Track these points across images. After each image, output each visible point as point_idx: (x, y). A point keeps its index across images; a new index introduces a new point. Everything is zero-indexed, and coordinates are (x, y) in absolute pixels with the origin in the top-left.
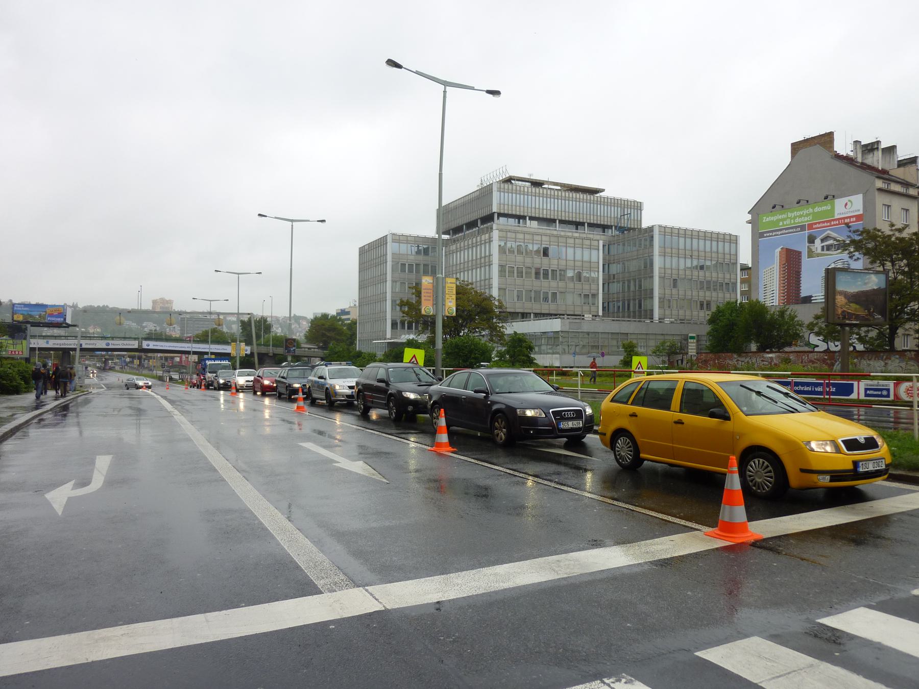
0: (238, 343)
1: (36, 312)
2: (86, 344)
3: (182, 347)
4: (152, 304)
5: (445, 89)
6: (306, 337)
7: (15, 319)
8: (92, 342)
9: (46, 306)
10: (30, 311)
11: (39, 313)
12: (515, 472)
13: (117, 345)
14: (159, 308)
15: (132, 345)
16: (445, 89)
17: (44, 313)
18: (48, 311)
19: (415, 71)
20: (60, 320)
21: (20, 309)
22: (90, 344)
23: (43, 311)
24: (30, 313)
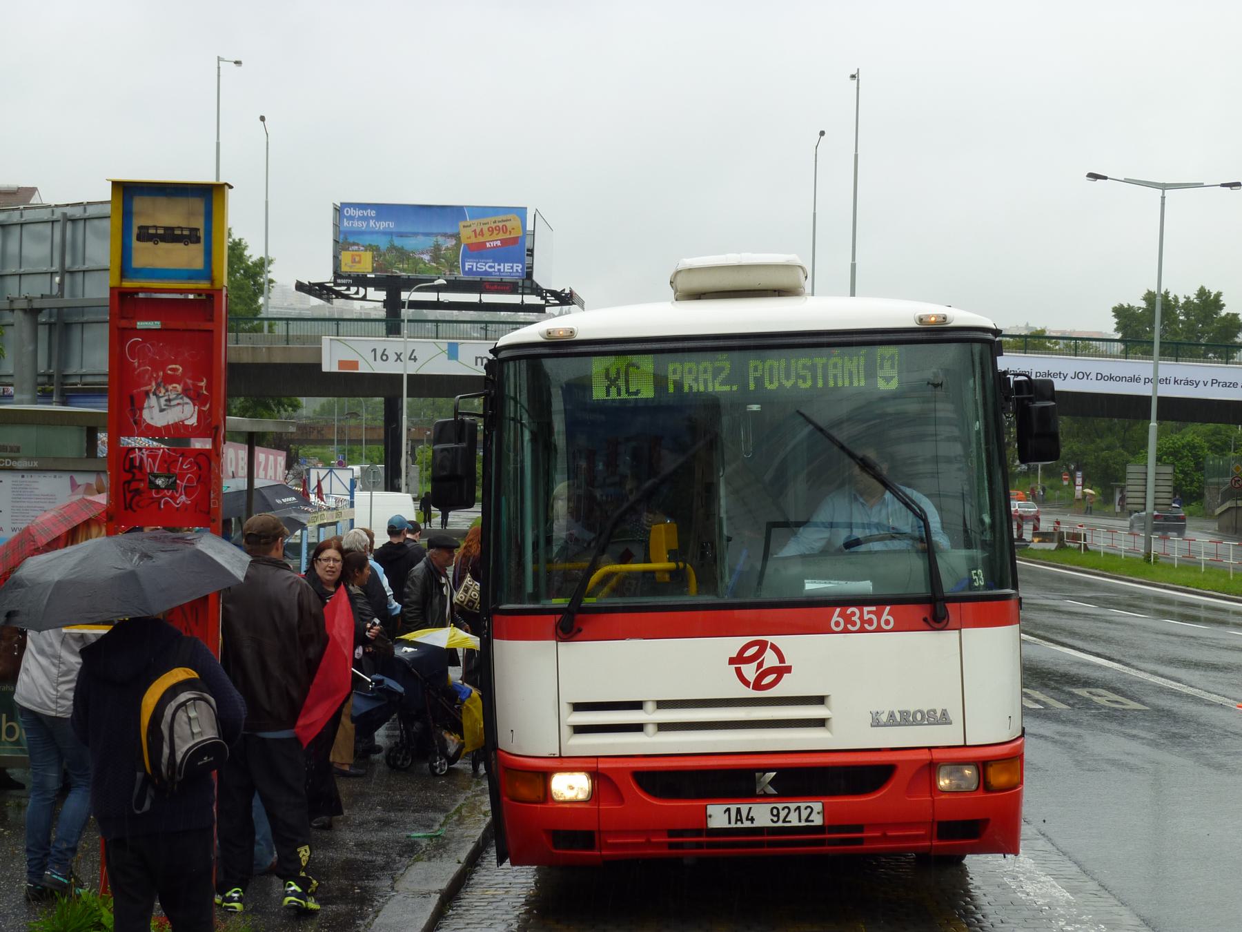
1: (421, 238)
5: (1163, 193)
6: (471, 506)
7: (345, 269)
10: (401, 235)
11: (430, 242)
16: (1163, 193)
17: (451, 243)
18: (467, 236)
19: (1123, 179)
20: (510, 270)
23: (445, 235)
24: (398, 242)
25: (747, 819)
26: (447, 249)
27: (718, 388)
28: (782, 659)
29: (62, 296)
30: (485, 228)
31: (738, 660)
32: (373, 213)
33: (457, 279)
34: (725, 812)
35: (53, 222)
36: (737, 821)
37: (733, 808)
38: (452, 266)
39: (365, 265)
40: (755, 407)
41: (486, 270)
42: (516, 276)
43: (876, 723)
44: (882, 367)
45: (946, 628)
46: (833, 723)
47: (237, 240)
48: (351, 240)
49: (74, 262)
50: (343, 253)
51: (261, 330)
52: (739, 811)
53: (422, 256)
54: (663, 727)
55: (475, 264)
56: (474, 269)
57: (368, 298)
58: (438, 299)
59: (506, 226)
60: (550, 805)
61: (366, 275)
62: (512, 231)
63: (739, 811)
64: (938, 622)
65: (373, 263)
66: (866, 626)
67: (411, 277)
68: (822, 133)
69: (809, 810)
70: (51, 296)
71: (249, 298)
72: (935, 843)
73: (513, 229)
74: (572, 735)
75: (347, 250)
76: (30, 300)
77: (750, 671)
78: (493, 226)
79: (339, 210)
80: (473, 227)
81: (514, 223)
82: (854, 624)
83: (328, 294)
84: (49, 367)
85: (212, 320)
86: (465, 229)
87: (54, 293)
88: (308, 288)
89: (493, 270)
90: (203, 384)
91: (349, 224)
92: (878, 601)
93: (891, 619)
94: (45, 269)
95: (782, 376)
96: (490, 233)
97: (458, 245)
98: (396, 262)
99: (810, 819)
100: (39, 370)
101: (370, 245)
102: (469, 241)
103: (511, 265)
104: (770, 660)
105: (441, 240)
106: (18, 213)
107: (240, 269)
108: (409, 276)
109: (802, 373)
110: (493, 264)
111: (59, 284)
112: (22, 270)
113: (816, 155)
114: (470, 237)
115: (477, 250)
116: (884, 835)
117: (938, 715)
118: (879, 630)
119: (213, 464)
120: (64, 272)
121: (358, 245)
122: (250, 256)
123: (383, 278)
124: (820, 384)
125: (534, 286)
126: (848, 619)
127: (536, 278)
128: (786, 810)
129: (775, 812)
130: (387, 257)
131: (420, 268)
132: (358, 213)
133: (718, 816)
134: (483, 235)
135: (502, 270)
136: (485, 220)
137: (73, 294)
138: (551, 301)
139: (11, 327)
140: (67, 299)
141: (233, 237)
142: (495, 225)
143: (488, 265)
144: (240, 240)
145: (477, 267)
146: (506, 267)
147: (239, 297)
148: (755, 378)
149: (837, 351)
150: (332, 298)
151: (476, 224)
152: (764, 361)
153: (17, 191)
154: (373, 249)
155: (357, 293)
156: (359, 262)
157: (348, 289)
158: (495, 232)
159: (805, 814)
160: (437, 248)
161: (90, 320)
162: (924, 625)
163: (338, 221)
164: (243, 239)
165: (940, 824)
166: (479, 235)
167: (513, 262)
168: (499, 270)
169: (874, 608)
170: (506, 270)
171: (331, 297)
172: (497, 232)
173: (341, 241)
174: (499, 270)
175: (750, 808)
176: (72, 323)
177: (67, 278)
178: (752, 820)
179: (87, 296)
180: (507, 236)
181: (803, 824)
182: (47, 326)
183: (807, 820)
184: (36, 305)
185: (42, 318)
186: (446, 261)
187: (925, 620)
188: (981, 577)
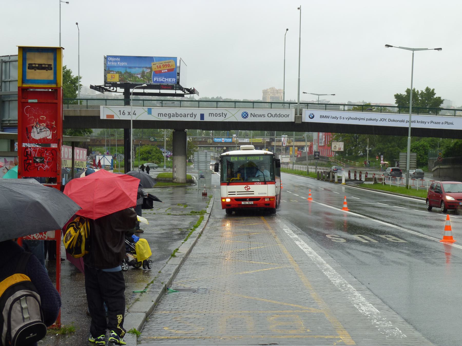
0: (294, 147)
1: (137, 69)
2: (211, 114)
3: (371, 120)
4: (262, 93)
7: (108, 80)
8: (219, 111)
9: (151, 59)
11: (140, 70)
12: (401, 228)
13: (260, 116)
14: (269, 99)
15: (284, 116)
17: (149, 70)
18: (154, 68)
20: (171, 81)
21: (115, 64)
22: (216, 115)
23: (146, 68)
24: (129, 70)
26: (147, 73)
30: (161, 65)
38: (149, 79)
39: (116, 79)
47: (68, 70)
48: (111, 69)
49: (6, 78)
50: (108, 74)
51: (77, 104)
53: (138, 76)
55: (158, 78)
56: (157, 81)
73: (172, 65)
78: (164, 64)
79: (106, 58)
80: (157, 65)
81: (172, 63)
83: (102, 90)
90: (54, 123)
97: (151, 71)
102: (155, 70)
105: (145, 69)
107: (69, 80)
115: (158, 73)
121: (113, 71)
132: (113, 59)
134: (160, 68)
135: (168, 81)
137: (5, 90)
141: (67, 69)
142: (165, 64)
145: (158, 80)
146: (169, 80)
147: (69, 91)
150: (104, 91)
151: (158, 63)
154: (120, 73)
155: (113, 89)
156: (114, 78)
157: (110, 88)
158: (165, 66)
160: (143, 72)
168: (167, 81)
170: (169, 81)
173: (107, 70)
174: (167, 81)
180: (170, 68)
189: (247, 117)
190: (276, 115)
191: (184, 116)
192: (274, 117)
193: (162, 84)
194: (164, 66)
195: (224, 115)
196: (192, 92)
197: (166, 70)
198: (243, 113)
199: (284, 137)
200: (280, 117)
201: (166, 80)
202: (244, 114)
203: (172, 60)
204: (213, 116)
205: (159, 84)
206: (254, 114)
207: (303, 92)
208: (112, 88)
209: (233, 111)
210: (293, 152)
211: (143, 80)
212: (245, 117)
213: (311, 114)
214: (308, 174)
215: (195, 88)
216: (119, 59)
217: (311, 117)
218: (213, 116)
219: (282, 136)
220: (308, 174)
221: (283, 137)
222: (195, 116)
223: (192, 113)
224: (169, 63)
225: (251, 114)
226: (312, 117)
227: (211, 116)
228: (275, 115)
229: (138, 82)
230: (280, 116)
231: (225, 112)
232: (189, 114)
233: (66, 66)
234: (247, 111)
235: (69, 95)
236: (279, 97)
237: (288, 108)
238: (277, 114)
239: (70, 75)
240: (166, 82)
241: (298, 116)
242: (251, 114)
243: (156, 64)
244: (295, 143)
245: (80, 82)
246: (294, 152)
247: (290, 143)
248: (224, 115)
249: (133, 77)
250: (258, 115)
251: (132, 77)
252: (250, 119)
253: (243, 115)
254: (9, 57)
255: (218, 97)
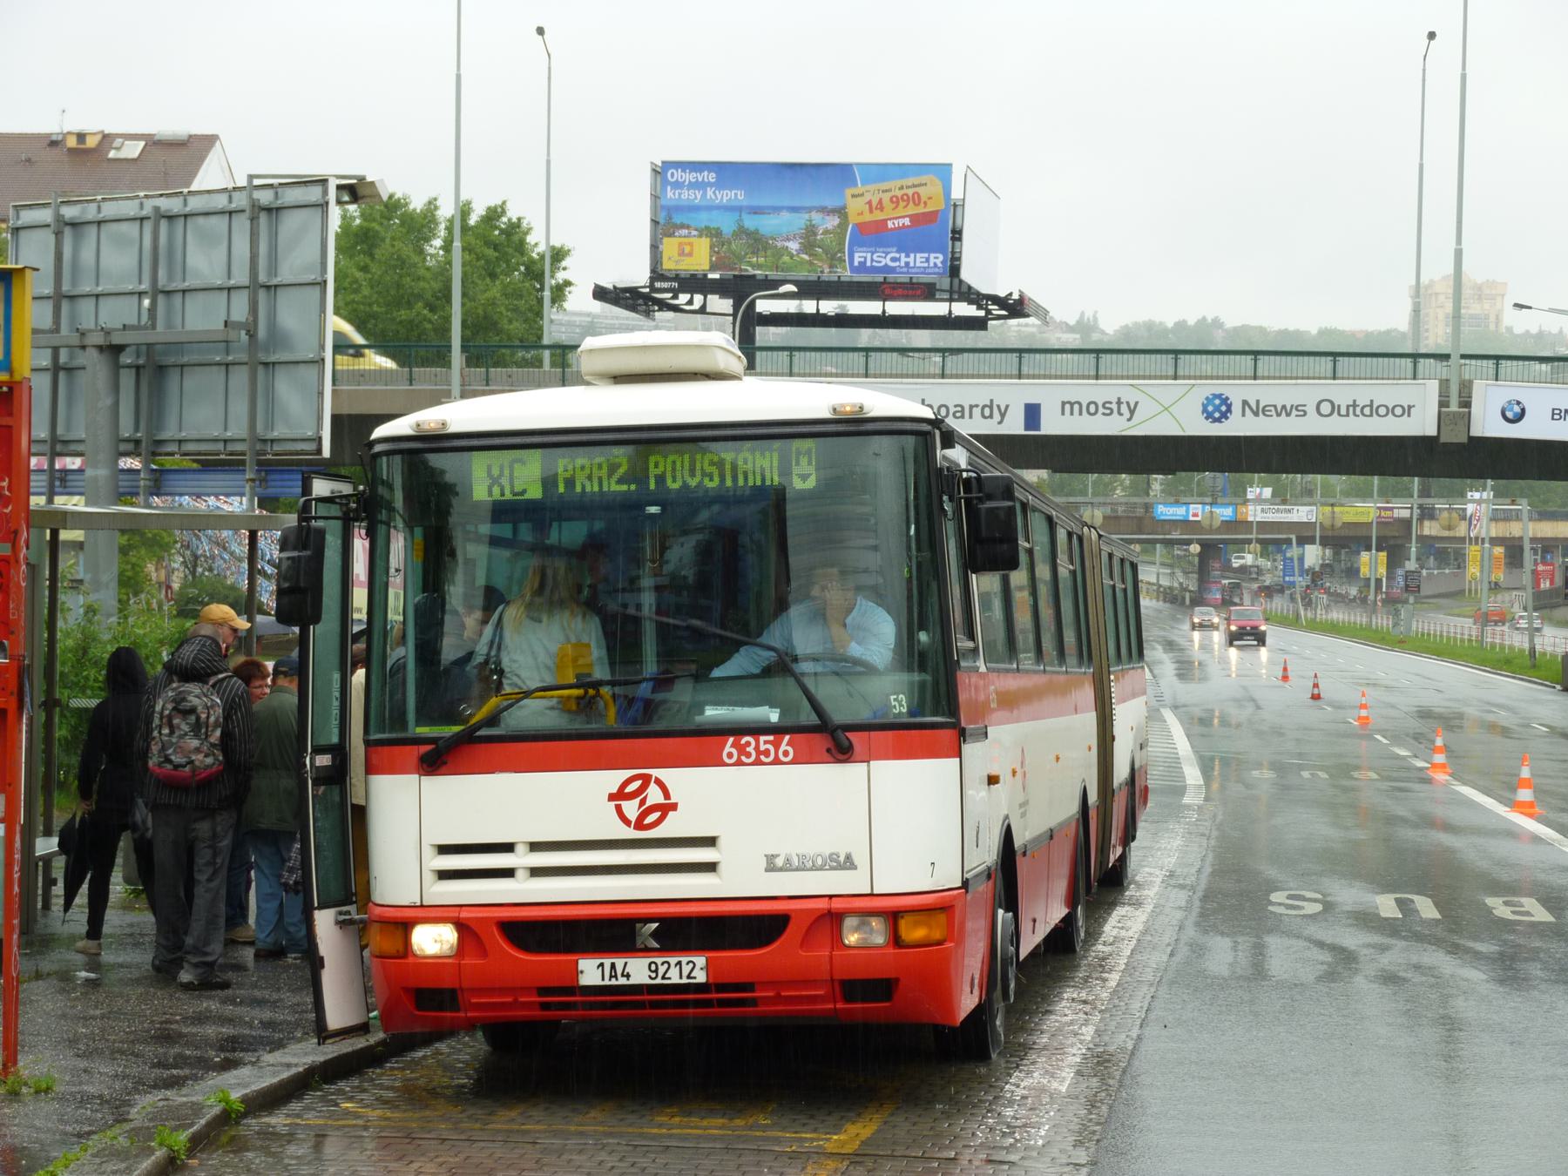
0: (1374, 551)
1: (786, 215)
2: (1068, 406)
7: (668, 265)
9: (838, 174)
10: (756, 211)
11: (799, 222)
13: (1284, 411)
15: (1390, 411)
17: (832, 222)
18: (857, 210)
20: (926, 263)
21: (694, 196)
22: (1092, 409)
24: (750, 222)
25: (623, 975)
26: (826, 232)
27: (615, 487)
28: (667, 795)
29: (154, 327)
30: (886, 197)
31: (619, 796)
32: (712, 177)
33: (842, 279)
34: (598, 967)
35: (142, 219)
36: (611, 977)
37: (607, 962)
38: (834, 259)
39: (698, 258)
40: (653, 510)
41: (886, 264)
42: (934, 274)
43: (771, 867)
44: (798, 463)
45: (852, 759)
46: (721, 868)
47: (514, 220)
48: (678, 219)
49: (170, 278)
50: (665, 240)
51: (540, 365)
52: (613, 966)
53: (787, 244)
54: (536, 872)
55: (869, 255)
56: (868, 264)
57: (708, 310)
58: (818, 310)
59: (918, 195)
60: (410, 960)
61: (705, 275)
62: (929, 202)
63: (613, 966)
64: (844, 754)
65: (711, 256)
66: (762, 757)
67: (769, 278)
68: (1432, 36)
69: (691, 965)
70: (133, 328)
71: (531, 309)
72: (839, 1006)
73: (930, 198)
74: (435, 882)
75: (671, 235)
76: (107, 332)
77: (631, 809)
78: (899, 193)
79: (660, 172)
80: (867, 197)
81: (931, 189)
82: (748, 755)
83: (646, 304)
84: (137, 429)
85: (10, 414)
86: (855, 199)
87: (143, 323)
88: (613, 295)
89: (897, 264)
90: (5, 484)
91: (674, 194)
92: (777, 731)
93: (790, 750)
94: (131, 287)
95: (686, 473)
96: (894, 205)
97: (843, 226)
98: (747, 254)
99: (692, 975)
100: (120, 433)
101: (707, 228)
102: (860, 219)
103: (926, 255)
104: (654, 795)
105: (816, 217)
106: (93, 206)
107: (518, 264)
108: (766, 276)
109: (708, 469)
110: (897, 255)
111: (149, 310)
112: (100, 289)
113: (1424, 70)
114: (862, 213)
115: (874, 233)
116: (778, 995)
117: (842, 859)
118: (777, 762)
119: (12, 571)
120: (156, 292)
121: (688, 227)
122: (536, 244)
123: (729, 280)
124: (729, 483)
125: (964, 289)
126: (742, 750)
127: (966, 275)
128: (666, 966)
129: (653, 967)
130: (734, 246)
131: (784, 263)
132: (689, 177)
133: (591, 971)
134: (882, 209)
135: (912, 264)
136: (885, 186)
137: (169, 325)
138: (994, 312)
139: (82, 371)
140: (160, 334)
141: (509, 214)
142: (902, 192)
143: (889, 257)
144: (519, 219)
145: (872, 260)
146: (918, 260)
147: (516, 310)
148: (656, 476)
149: (748, 444)
150: (654, 311)
151: (872, 192)
152: (666, 457)
153: (188, 141)
154: (713, 234)
155: (690, 302)
156: (690, 254)
157: (675, 297)
158: (902, 204)
159: (686, 969)
160: (811, 230)
161: (192, 362)
162: (826, 755)
163: (659, 188)
164: (524, 218)
165: (843, 983)
166: (876, 208)
167: (930, 251)
168: (907, 264)
169: (771, 738)
170: (918, 264)
171: (651, 308)
172: (905, 203)
173: (662, 221)
174: (907, 264)
175: (626, 964)
176: (166, 366)
177: (161, 299)
178: (628, 976)
179: (190, 326)
180: (921, 210)
181: (685, 981)
182: (134, 370)
183: (689, 977)
184: (117, 340)
185: (126, 359)
186: (826, 252)
187: (828, 750)
188: (904, 703)
189: (1224, 416)
190: (1355, 405)
191: (954, 414)
192: (1348, 415)
193: (891, 277)
194: (898, 202)
195: (1124, 409)
196: (1015, 308)
197: (903, 217)
198: (1207, 398)
199: (1479, 502)
200: (1371, 415)
201: (904, 259)
202: (1214, 405)
203: (932, 177)
204: (1081, 414)
205: (879, 278)
206: (1258, 402)
207: (1516, 305)
208: (683, 298)
209: (1167, 390)
210: (1482, 567)
211: (811, 263)
212: (1217, 415)
213: (1509, 402)
214: (1534, 666)
215: (1029, 293)
216: (711, 177)
217: (1509, 415)
218: (1081, 414)
219: (1469, 494)
220: (1534, 666)
221: (1473, 501)
222: (1003, 415)
223: (992, 401)
224: (917, 189)
225: (1245, 403)
226: (1516, 414)
227: (1072, 414)
228: (1348, 407)
229: (789, 269)
230: (1373, 410)
231: (1130, 396)
232: (977, 406)
233: (504, 203)
234: (1227, 392)
235: (516, 327)
236: (1487, 317)
237: (1410, 374)
238: (1361, 403)
239: (522, 242)
240: (905, 270)
241: (1454, 413)
242: (1245, 403)
243: (862, 195)
244: (1531, 525)
245: (564, 269)
246: (1486, 563)
247: (1449, 528)
248: (1124, 409)
249: (769, 252)
250: (1275, 406)
251: (765, 249)
252: (1238, 426)
253: (1210, 408)
254: (181, 198)
255: (1204, 319)
